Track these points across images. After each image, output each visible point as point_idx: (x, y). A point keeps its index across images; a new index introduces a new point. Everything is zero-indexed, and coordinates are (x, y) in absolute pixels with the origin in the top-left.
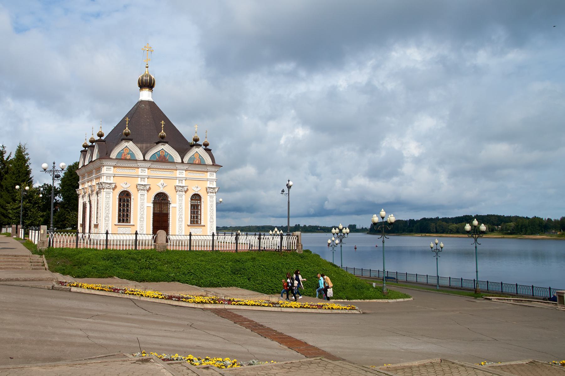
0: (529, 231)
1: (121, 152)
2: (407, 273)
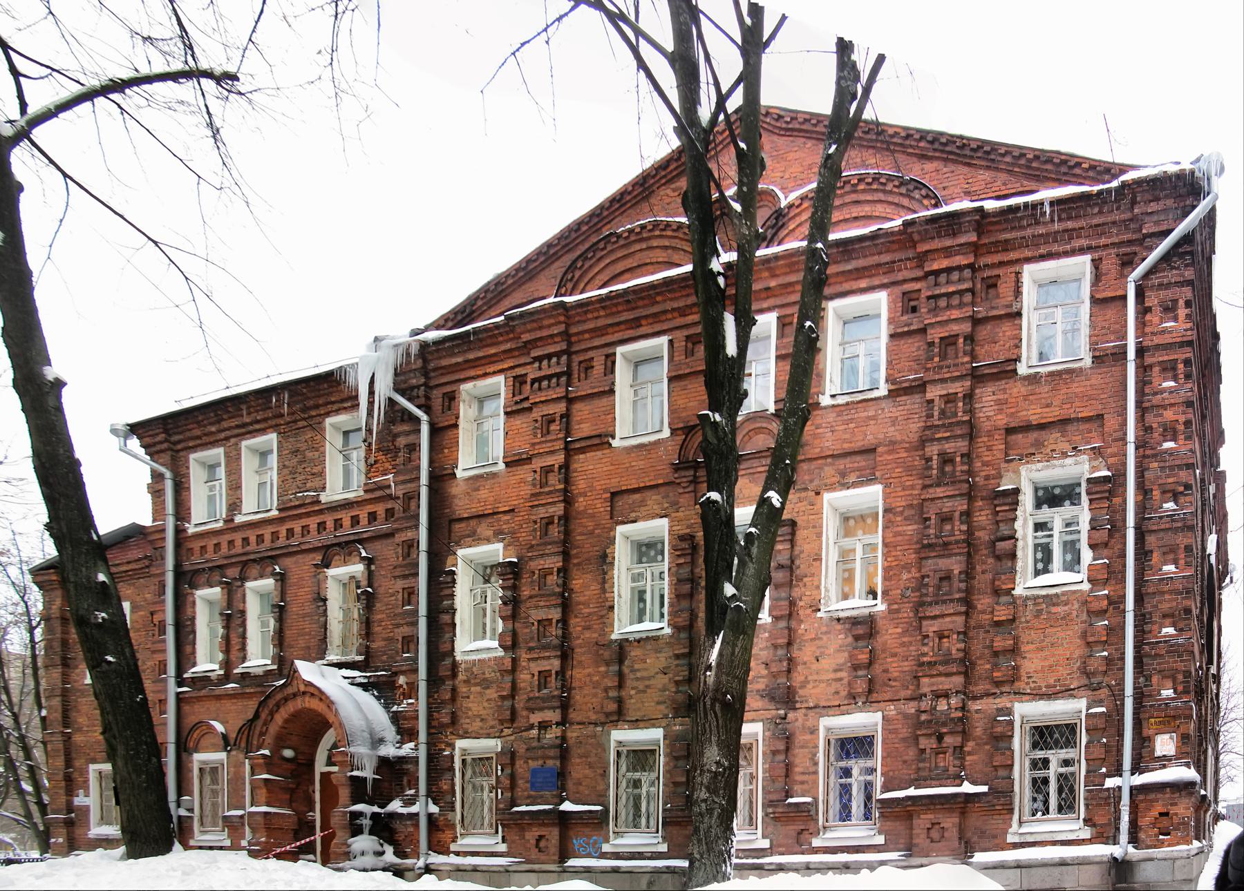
1: (789, 804)
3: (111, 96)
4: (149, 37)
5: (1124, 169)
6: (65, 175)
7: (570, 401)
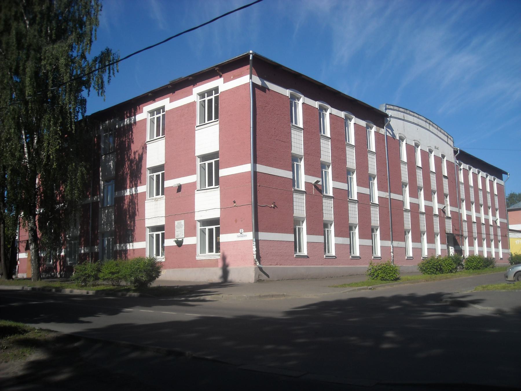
2: (261, 295)
4: (467, 269)
5: (464, 304)
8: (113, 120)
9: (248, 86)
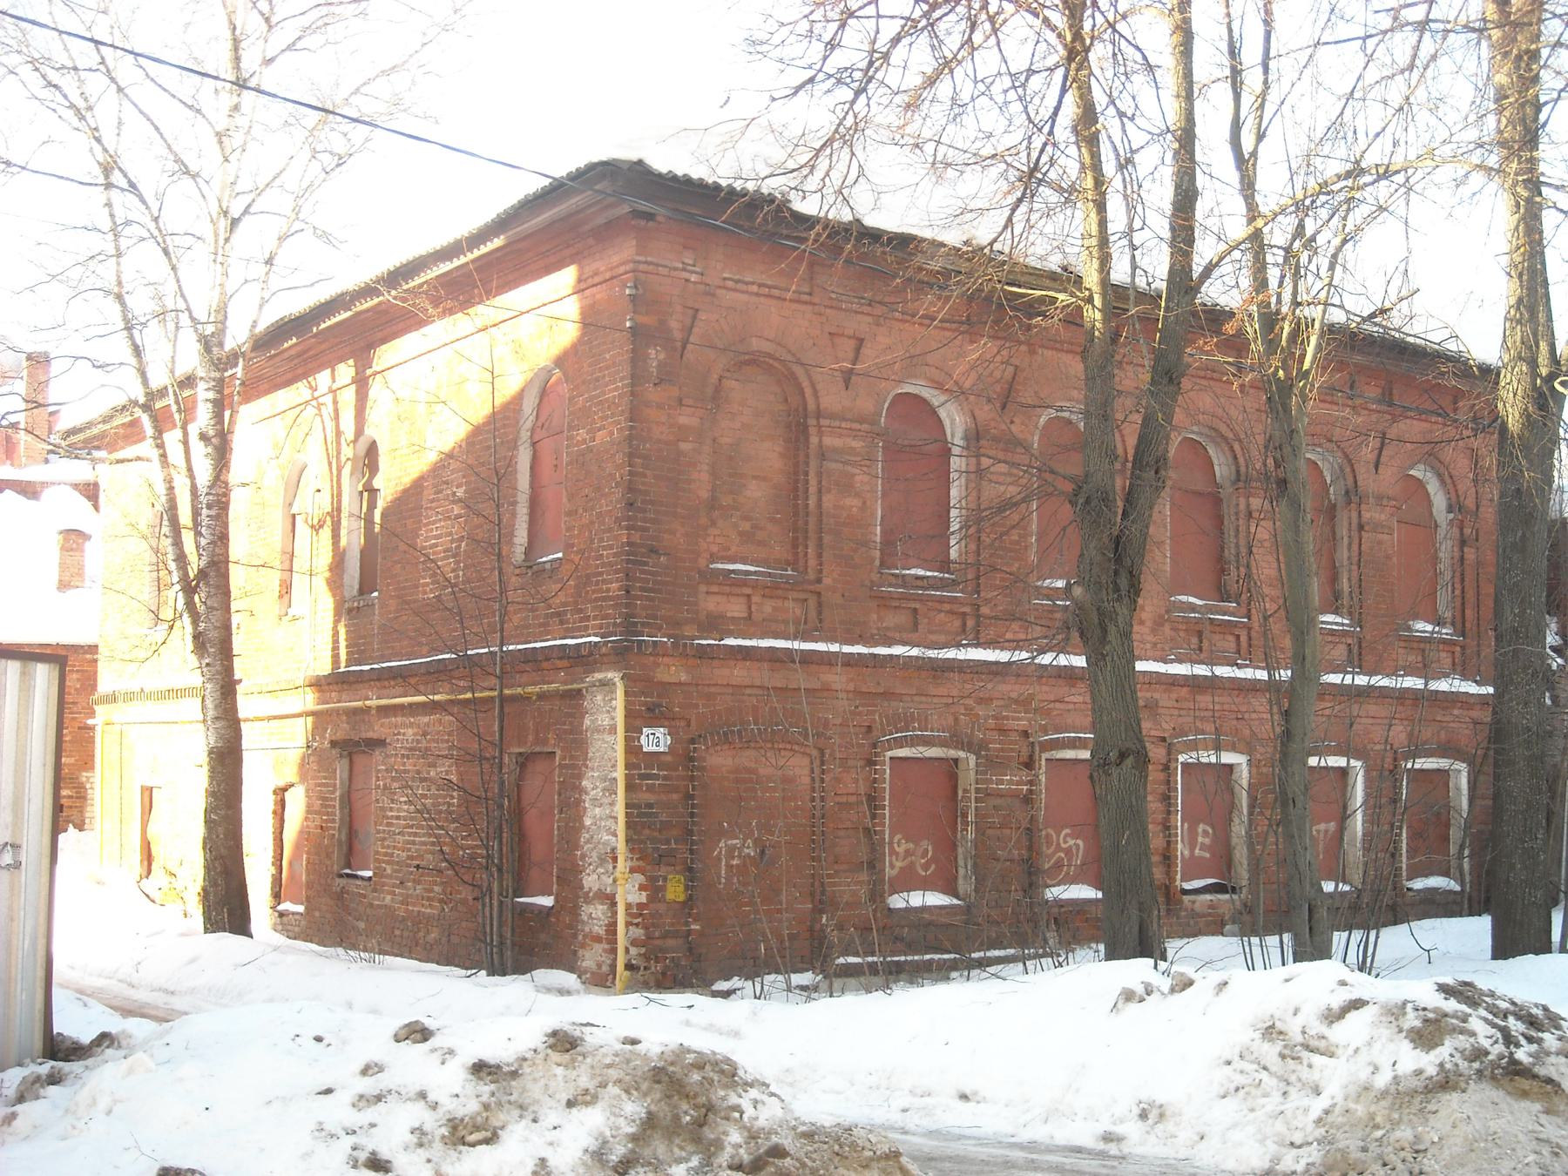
0: (1369, 659)
3: (547, 182)
6: (523, 313)
7: (932, 25)
8: (315, 330)
9: (25, 676)
